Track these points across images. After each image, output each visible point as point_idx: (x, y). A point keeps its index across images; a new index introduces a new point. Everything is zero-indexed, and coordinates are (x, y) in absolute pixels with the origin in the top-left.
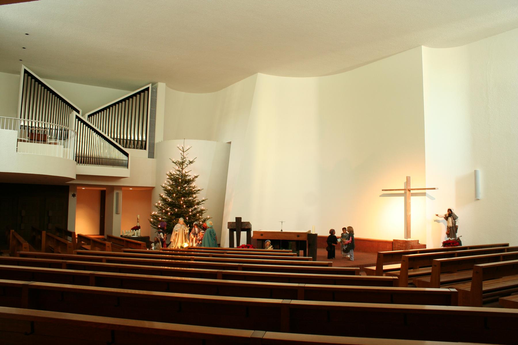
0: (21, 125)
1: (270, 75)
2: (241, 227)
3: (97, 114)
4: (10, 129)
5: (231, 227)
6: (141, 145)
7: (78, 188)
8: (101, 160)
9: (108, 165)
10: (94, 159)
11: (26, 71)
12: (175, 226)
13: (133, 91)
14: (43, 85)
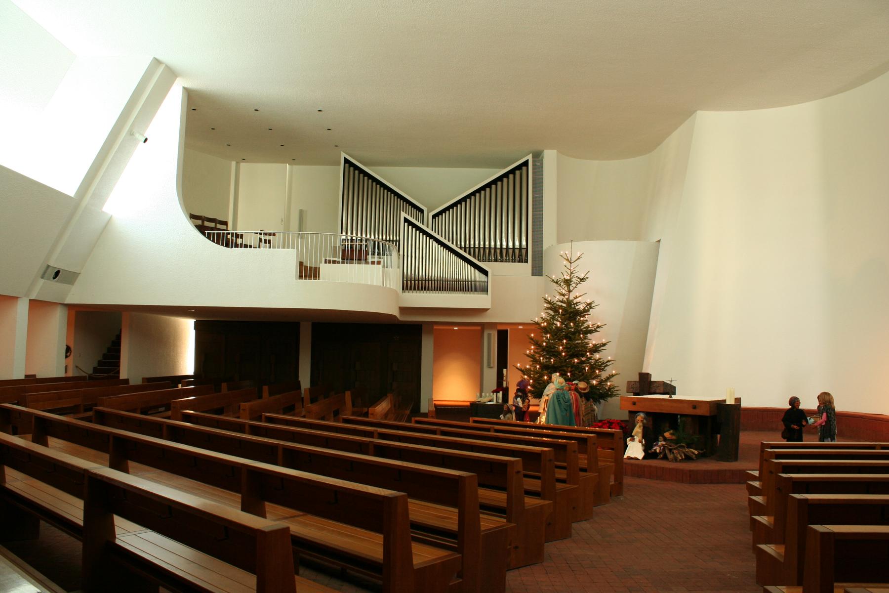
2: (649, 390)
4: (288, 248)
5: (632, 389)
6: (519, 256)
7: (435, 327)
8: (437, 283)
10: (433, 282)
11: (346, 161)
12: (547, 388)
13: (504, 168)
14: (370, 177)
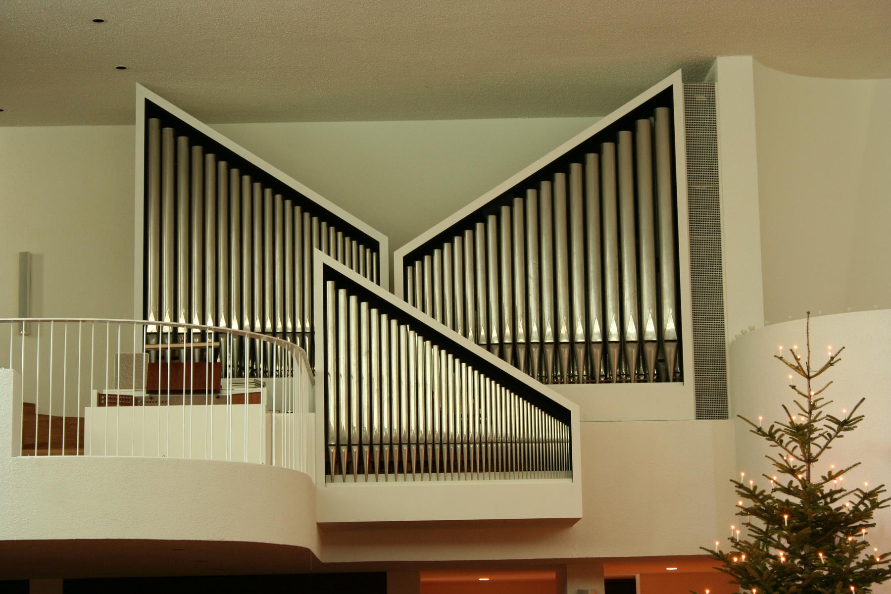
0: (147, 334)
1: (237, 123)
3: (446, 246)
9: (481, 470)
10: (414, 448)
11: (151, 109)
